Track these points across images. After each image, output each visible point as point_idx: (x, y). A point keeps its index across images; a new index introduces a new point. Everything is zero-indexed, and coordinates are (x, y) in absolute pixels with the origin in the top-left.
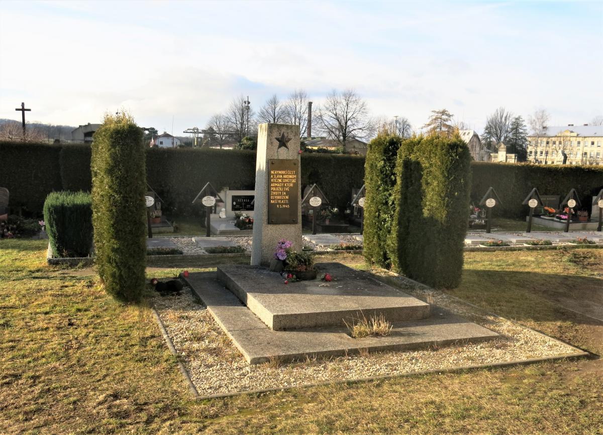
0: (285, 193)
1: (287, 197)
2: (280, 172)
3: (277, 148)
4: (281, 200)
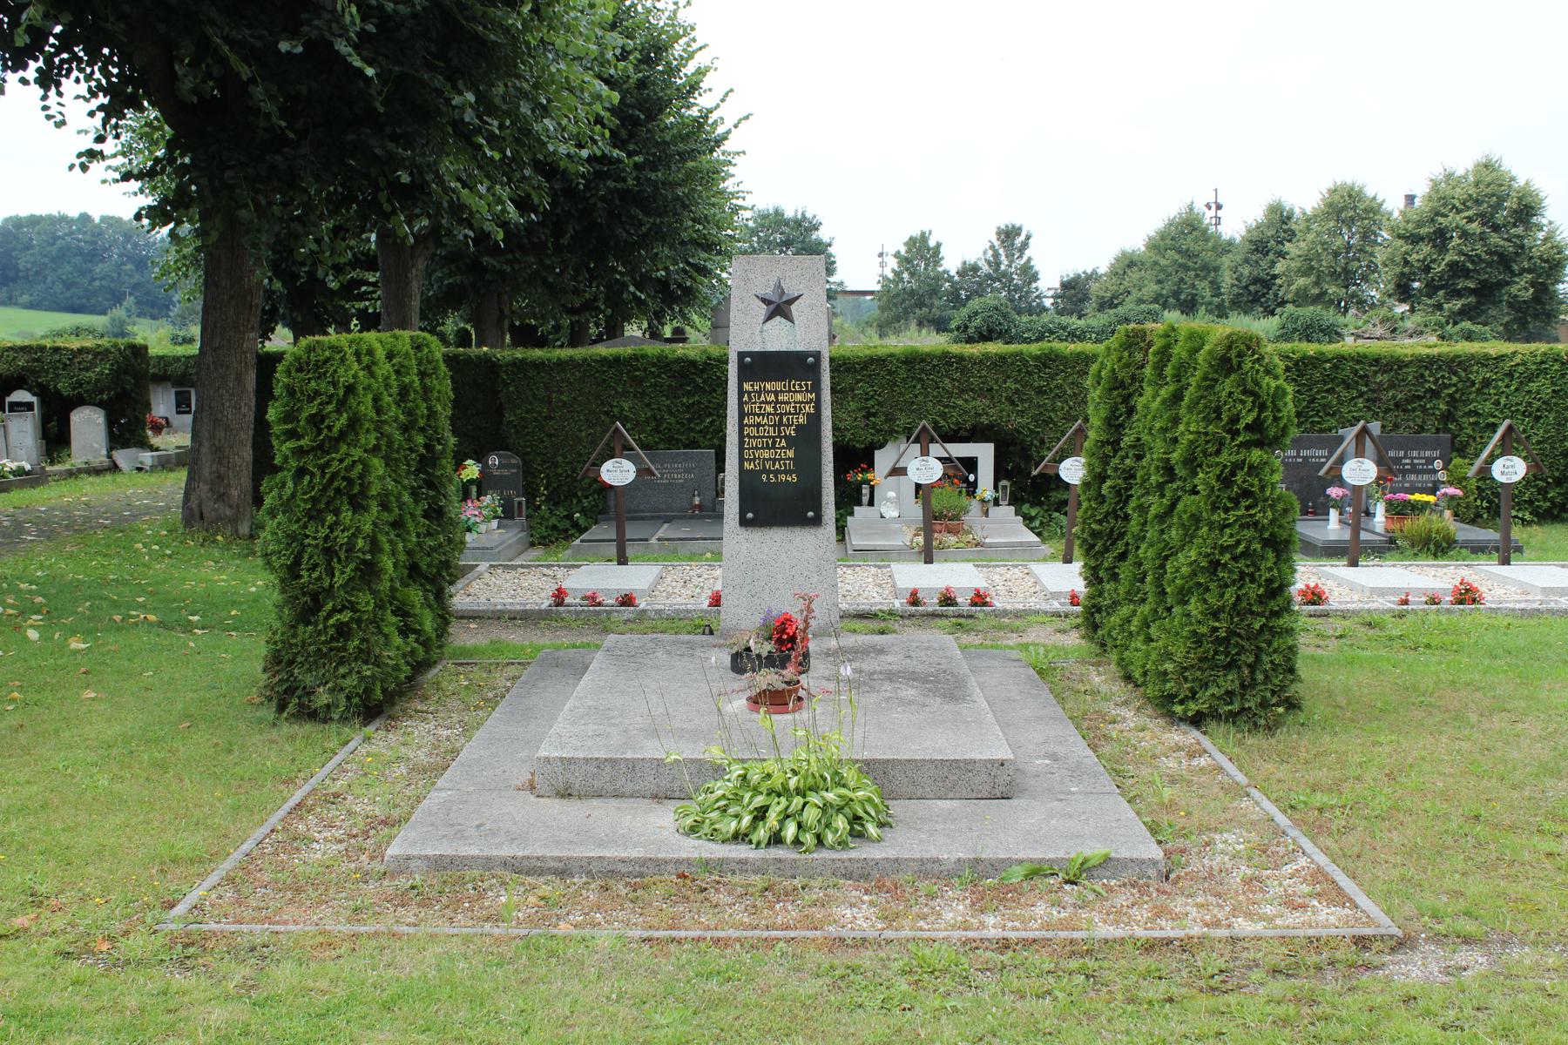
0: (783, 443)
1: (791, 454)
2: (768, 386)
3: (762, 318)
4: (774, 460)
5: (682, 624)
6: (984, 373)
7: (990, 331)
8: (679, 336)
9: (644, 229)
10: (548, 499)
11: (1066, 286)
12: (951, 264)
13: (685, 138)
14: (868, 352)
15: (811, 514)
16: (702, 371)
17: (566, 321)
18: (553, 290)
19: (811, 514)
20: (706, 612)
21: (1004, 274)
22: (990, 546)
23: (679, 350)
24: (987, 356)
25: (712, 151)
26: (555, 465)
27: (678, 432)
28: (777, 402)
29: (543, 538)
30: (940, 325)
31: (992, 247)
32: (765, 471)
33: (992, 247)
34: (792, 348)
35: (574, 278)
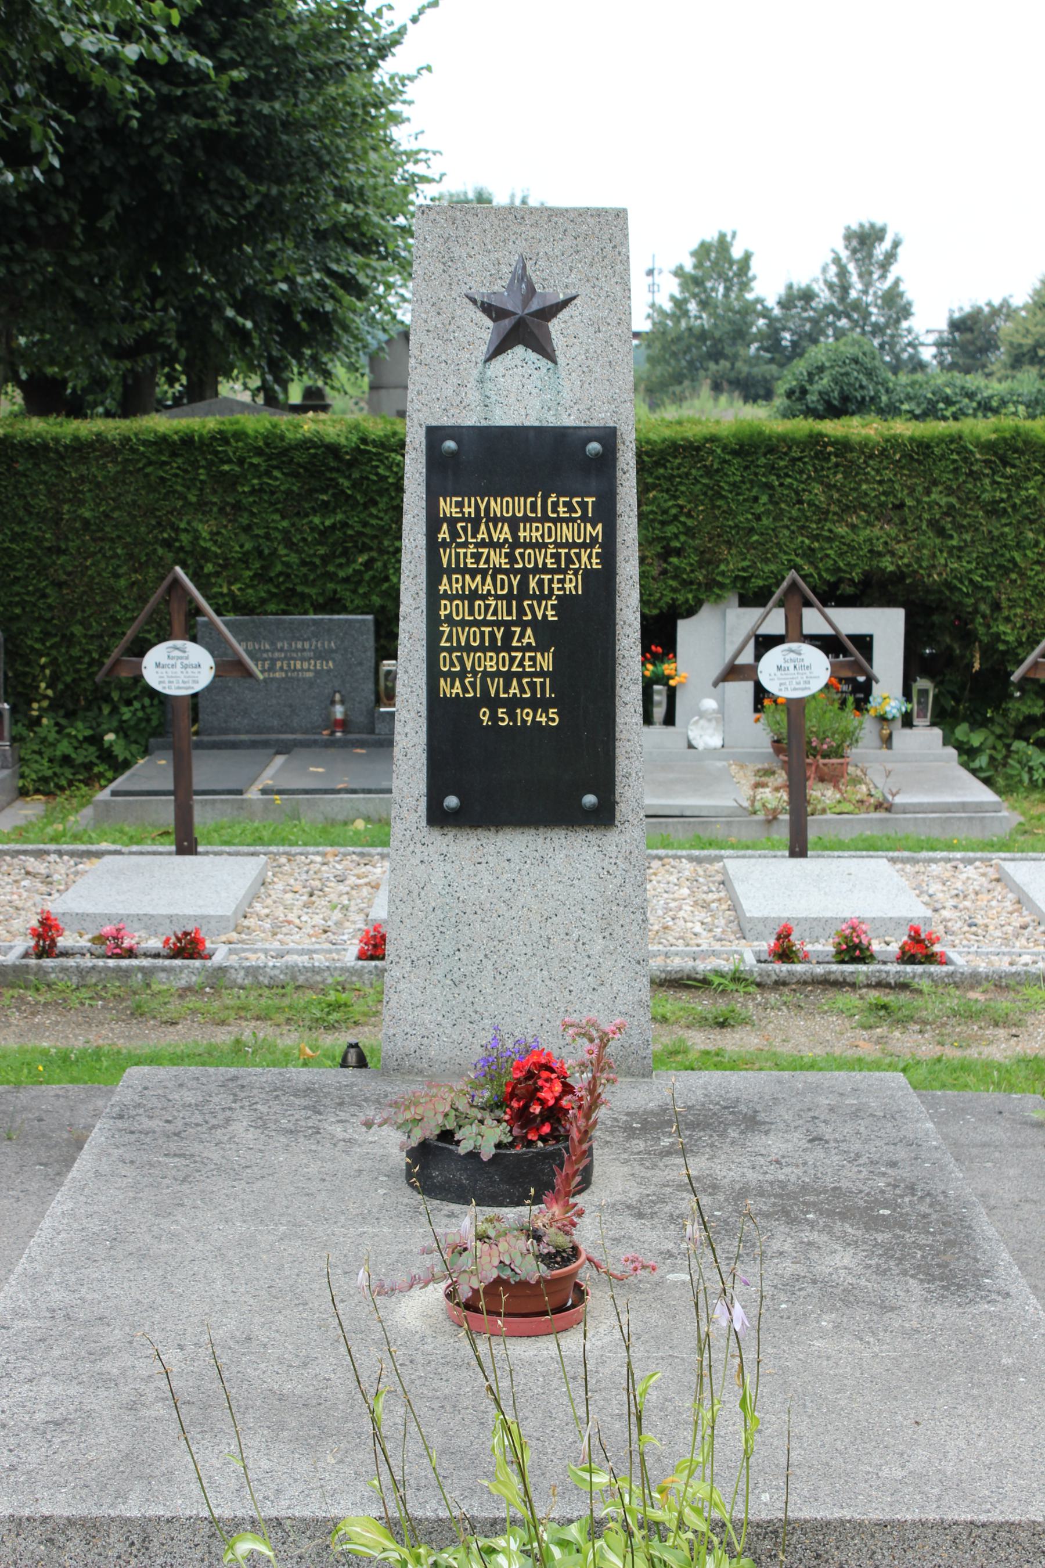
0: (529, 638)
4: (508, 677)
5: (301, 999)
6: (888, 474)
7: (845, 398)
8: (315, 401)
9: (249, 206)
10: (55, 706)
11: (956, 325)
12: (767, 288)
13: (323, 40)
14: (667, 433)
15: (590, 799)
16: (351, 464)
17: (109, 368)
18: (87, 315)
19: (590, 799)
20: (353, 972)
21: (856, 306)
22: (905, 809)
23: (309, 424)
24: (893, 442)
25: (372, 65)
26: (69, 640)
27: (305, 582)
28: (516, 543)
29: (45, 780)
30: (754, 390)
31: (837, 261)
32: (486, 700)
33: (837, 261)
34: (551, 420)
35: (126, 294)
